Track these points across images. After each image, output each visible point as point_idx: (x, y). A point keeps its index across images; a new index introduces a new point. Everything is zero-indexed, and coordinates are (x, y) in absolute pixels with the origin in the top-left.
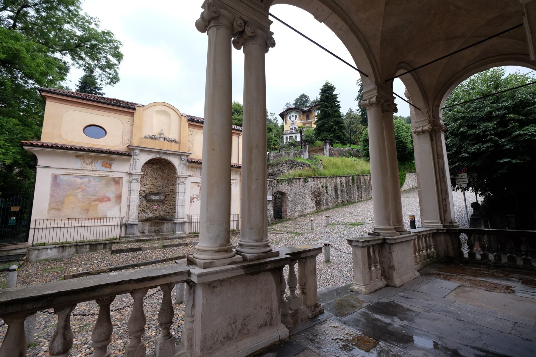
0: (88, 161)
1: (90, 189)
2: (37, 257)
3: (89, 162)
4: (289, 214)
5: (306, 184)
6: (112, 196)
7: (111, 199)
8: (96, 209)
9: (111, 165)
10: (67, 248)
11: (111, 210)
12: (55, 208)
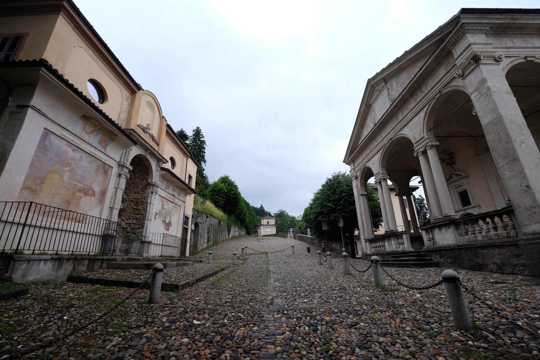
0: (89, 129)
1: (79, 171)
2: (24, 276)
3: (89, 131)
4: (248, 220)
5: (153, 242)
6: (97, 189)
7: (96, 194)
8: (78, 204)
9: (106, 146)
10: (65, 261)
11: (93, 210)
12: (30, 188)
